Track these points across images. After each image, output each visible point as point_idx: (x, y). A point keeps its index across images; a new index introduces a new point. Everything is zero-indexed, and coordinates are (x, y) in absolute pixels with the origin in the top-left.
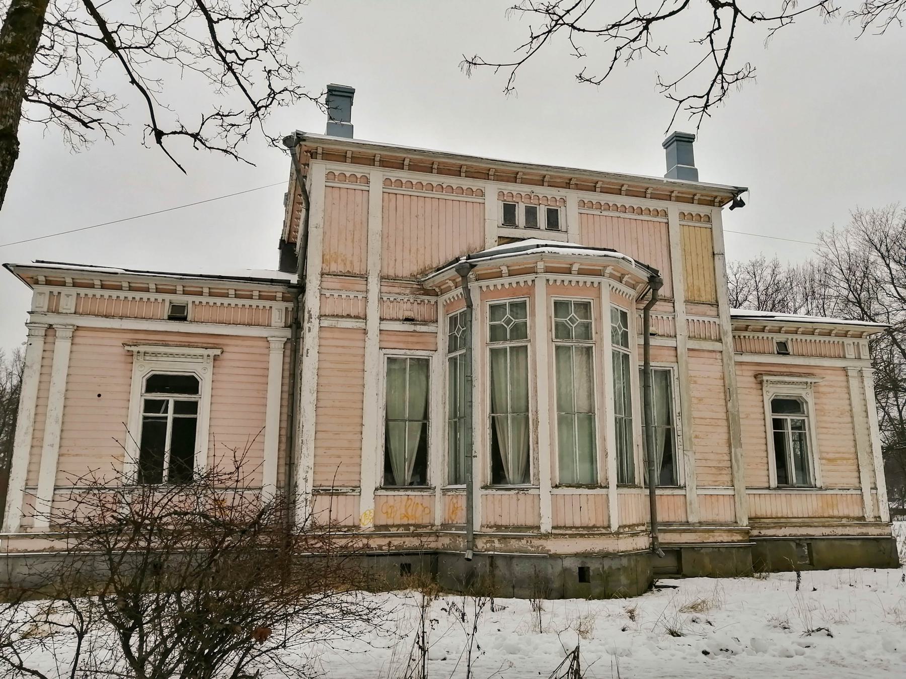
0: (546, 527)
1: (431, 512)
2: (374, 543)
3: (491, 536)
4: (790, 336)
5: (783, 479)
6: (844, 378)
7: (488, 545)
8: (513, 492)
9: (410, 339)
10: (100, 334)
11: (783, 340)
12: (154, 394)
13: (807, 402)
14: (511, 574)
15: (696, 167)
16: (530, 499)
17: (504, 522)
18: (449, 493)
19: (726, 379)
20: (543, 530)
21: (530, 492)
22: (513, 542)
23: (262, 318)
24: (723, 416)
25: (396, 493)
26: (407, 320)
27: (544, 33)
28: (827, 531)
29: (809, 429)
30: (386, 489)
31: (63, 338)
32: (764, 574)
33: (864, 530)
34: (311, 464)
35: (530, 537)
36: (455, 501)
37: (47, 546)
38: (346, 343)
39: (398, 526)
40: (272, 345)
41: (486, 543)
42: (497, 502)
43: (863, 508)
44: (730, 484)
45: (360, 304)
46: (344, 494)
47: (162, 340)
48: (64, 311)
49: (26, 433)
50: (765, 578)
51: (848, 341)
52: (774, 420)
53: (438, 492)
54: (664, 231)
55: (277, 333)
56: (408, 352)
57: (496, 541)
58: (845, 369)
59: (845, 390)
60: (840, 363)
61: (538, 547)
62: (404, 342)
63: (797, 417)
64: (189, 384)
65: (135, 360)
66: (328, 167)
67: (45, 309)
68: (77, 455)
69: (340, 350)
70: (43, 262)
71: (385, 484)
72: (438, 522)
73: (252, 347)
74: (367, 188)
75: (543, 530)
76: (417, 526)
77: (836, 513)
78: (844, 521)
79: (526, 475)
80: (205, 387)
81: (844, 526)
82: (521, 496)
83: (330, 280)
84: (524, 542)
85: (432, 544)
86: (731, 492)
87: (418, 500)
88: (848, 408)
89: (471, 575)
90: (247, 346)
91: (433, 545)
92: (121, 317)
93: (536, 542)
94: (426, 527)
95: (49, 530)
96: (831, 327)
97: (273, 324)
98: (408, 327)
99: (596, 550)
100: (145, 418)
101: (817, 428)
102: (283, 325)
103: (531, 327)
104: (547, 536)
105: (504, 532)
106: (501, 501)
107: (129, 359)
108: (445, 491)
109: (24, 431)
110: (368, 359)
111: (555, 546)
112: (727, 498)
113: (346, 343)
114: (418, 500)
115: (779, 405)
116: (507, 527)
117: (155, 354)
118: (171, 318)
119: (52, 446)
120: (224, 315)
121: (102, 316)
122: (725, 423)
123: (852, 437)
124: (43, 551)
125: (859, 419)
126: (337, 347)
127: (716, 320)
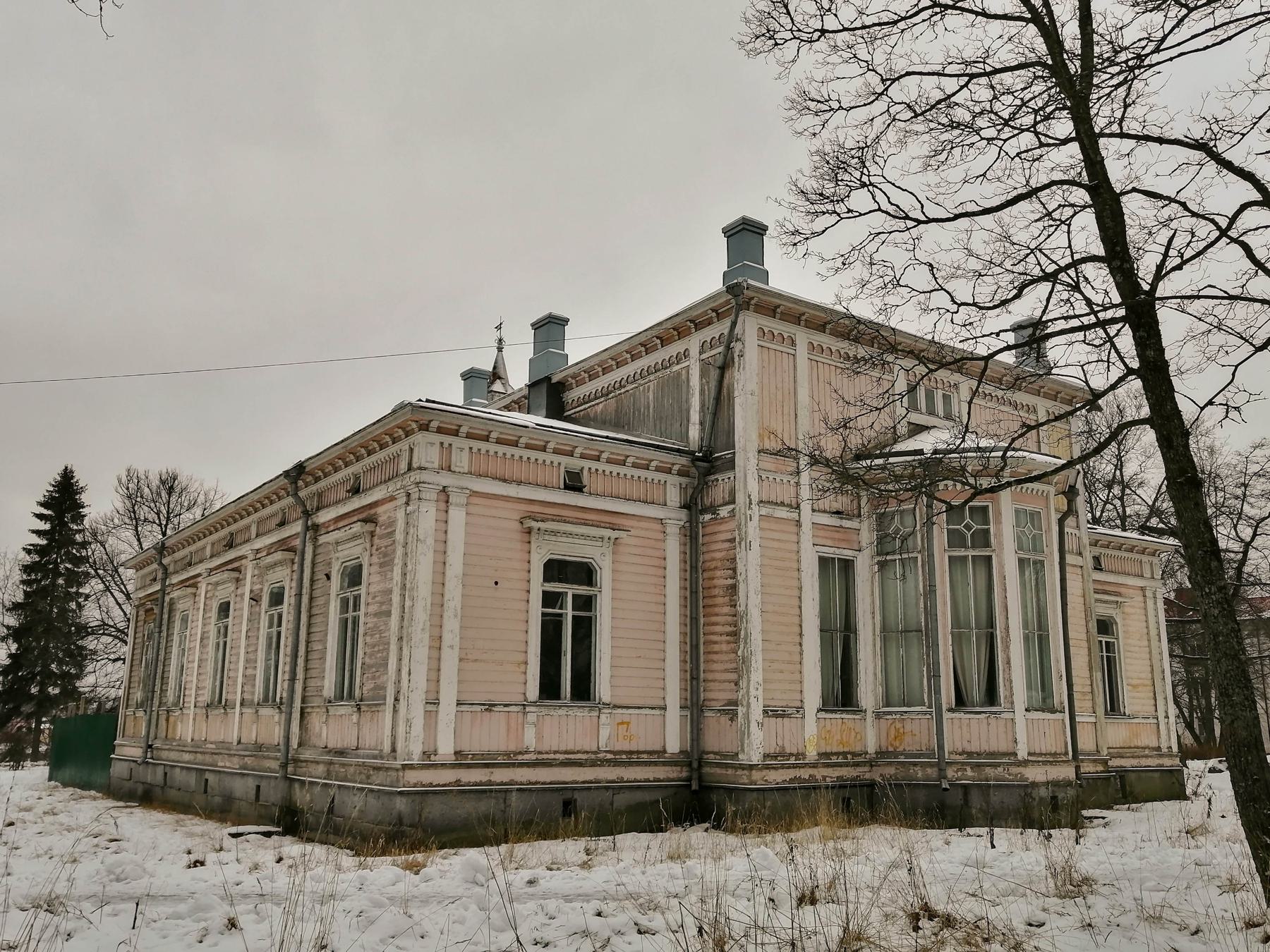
0: (1022, 754)
1: (863, 739)
2: (819, 773)
3: (963, 764)
4: (587, 464)
5: (549, 689)
6: (1141, 599)
7: (960, 773)
8: (983, 716)
9: (837, 535)
10: (495, 503)
11: (1097, 554)
12: (552, 584)
13: (1116, 623)
14: (988, 806)
15: (566, 351)
16: (1002, 723)
17: (974, 747)
18: (888, 717)
19: (1087, 597)
20: (1020, 757)
21: (1002, 716)
22: (988, 770)
23: (657, 495)
24: (1084, 636)
25: (833, 716)
26: (838, 513)
27: (1225, 292)
28: (1134, 762)
29: (1119, 652)
30: (826, 711)
31: (457, 505)
32: (1134, 806)
33: (1160, 761)
34: (760, 680)
35: (1008, 764)
36: (899, 725)
37: (453, 780)
38: (776, 535)
39: (838, 754)
40: (668, 530)
41: (957, 772)
42: (965, 728)
43: (1159, 737)
44: (1091, 710)
45: (793, 490)
46: (789, 716)
47: (558, 514)
48: (457, 470)
49: (423, 629)
50: (1136, 810)
51: (1145, 558)
52: (545, 593)
53: (869, 714)
54: (415, 460)
55: (672, 515)
56: (837, 551)
57: (968, 769)
58: (1143, 589)
59: (1143, 611)
60: (1139, 582)
61: (1016, 775)
62: (833, 539)
63: (583, 590)
64: (584, 573)
65: (533, 539)
66: (760, 321)
67: (436, 465)
68: (476, 660)
69: (776, 544)
70: (434, 402)
71: (540, 697)
72: (871, 749)
73: (647, 529)
74: (793, 352)
75: (1020, 757)
76: (854, 754)
77: (1139, 744)
78: (1147, 752)
79: (991, 696)
80: (605, 577)
81: (1147, 756)
82: (992, 721)
83: (765, 459)
84: (1000, 769)
85: (865, 773)
86: (1093, 720)
87: (851, 724)
88: (1145, 631)
89: (943, 807)
90: (642, 529)
91: (867, 776)
92: (519, 483)
93: (1014, 770)
94: (860, 755)
95: (454, 758)
96: (1122, 541)
97: (669, 503)
98: (834, 521)
99: (1061, 778)
100: (544, 614)
101: (1125, 651)
102: (678, 505)
103: (995, 535)
104: (1025, 763)
105: (977, 759)
106: (969, 725)
107: (526, 537)
108: (878, 716)
109: (421, 626)
110: (803, 553)
111: (1035, 774)
112: (1090, 725)
113: (776, 535)
114: (851, 724)
115: (556, 570)
116: (979, 754)
117: (555, 533)
118: (567, 487)
119: (452, 647)
120: (621, 487)
121: (500, 479)
122: (1085, 644)
123: (1148, 662)
124: (550, 783)
125: (1154, 643)
126: (773, 540)
127: (1076, 532)
